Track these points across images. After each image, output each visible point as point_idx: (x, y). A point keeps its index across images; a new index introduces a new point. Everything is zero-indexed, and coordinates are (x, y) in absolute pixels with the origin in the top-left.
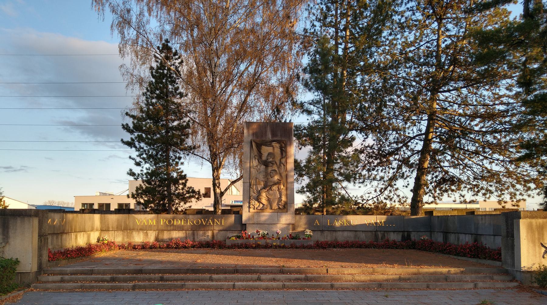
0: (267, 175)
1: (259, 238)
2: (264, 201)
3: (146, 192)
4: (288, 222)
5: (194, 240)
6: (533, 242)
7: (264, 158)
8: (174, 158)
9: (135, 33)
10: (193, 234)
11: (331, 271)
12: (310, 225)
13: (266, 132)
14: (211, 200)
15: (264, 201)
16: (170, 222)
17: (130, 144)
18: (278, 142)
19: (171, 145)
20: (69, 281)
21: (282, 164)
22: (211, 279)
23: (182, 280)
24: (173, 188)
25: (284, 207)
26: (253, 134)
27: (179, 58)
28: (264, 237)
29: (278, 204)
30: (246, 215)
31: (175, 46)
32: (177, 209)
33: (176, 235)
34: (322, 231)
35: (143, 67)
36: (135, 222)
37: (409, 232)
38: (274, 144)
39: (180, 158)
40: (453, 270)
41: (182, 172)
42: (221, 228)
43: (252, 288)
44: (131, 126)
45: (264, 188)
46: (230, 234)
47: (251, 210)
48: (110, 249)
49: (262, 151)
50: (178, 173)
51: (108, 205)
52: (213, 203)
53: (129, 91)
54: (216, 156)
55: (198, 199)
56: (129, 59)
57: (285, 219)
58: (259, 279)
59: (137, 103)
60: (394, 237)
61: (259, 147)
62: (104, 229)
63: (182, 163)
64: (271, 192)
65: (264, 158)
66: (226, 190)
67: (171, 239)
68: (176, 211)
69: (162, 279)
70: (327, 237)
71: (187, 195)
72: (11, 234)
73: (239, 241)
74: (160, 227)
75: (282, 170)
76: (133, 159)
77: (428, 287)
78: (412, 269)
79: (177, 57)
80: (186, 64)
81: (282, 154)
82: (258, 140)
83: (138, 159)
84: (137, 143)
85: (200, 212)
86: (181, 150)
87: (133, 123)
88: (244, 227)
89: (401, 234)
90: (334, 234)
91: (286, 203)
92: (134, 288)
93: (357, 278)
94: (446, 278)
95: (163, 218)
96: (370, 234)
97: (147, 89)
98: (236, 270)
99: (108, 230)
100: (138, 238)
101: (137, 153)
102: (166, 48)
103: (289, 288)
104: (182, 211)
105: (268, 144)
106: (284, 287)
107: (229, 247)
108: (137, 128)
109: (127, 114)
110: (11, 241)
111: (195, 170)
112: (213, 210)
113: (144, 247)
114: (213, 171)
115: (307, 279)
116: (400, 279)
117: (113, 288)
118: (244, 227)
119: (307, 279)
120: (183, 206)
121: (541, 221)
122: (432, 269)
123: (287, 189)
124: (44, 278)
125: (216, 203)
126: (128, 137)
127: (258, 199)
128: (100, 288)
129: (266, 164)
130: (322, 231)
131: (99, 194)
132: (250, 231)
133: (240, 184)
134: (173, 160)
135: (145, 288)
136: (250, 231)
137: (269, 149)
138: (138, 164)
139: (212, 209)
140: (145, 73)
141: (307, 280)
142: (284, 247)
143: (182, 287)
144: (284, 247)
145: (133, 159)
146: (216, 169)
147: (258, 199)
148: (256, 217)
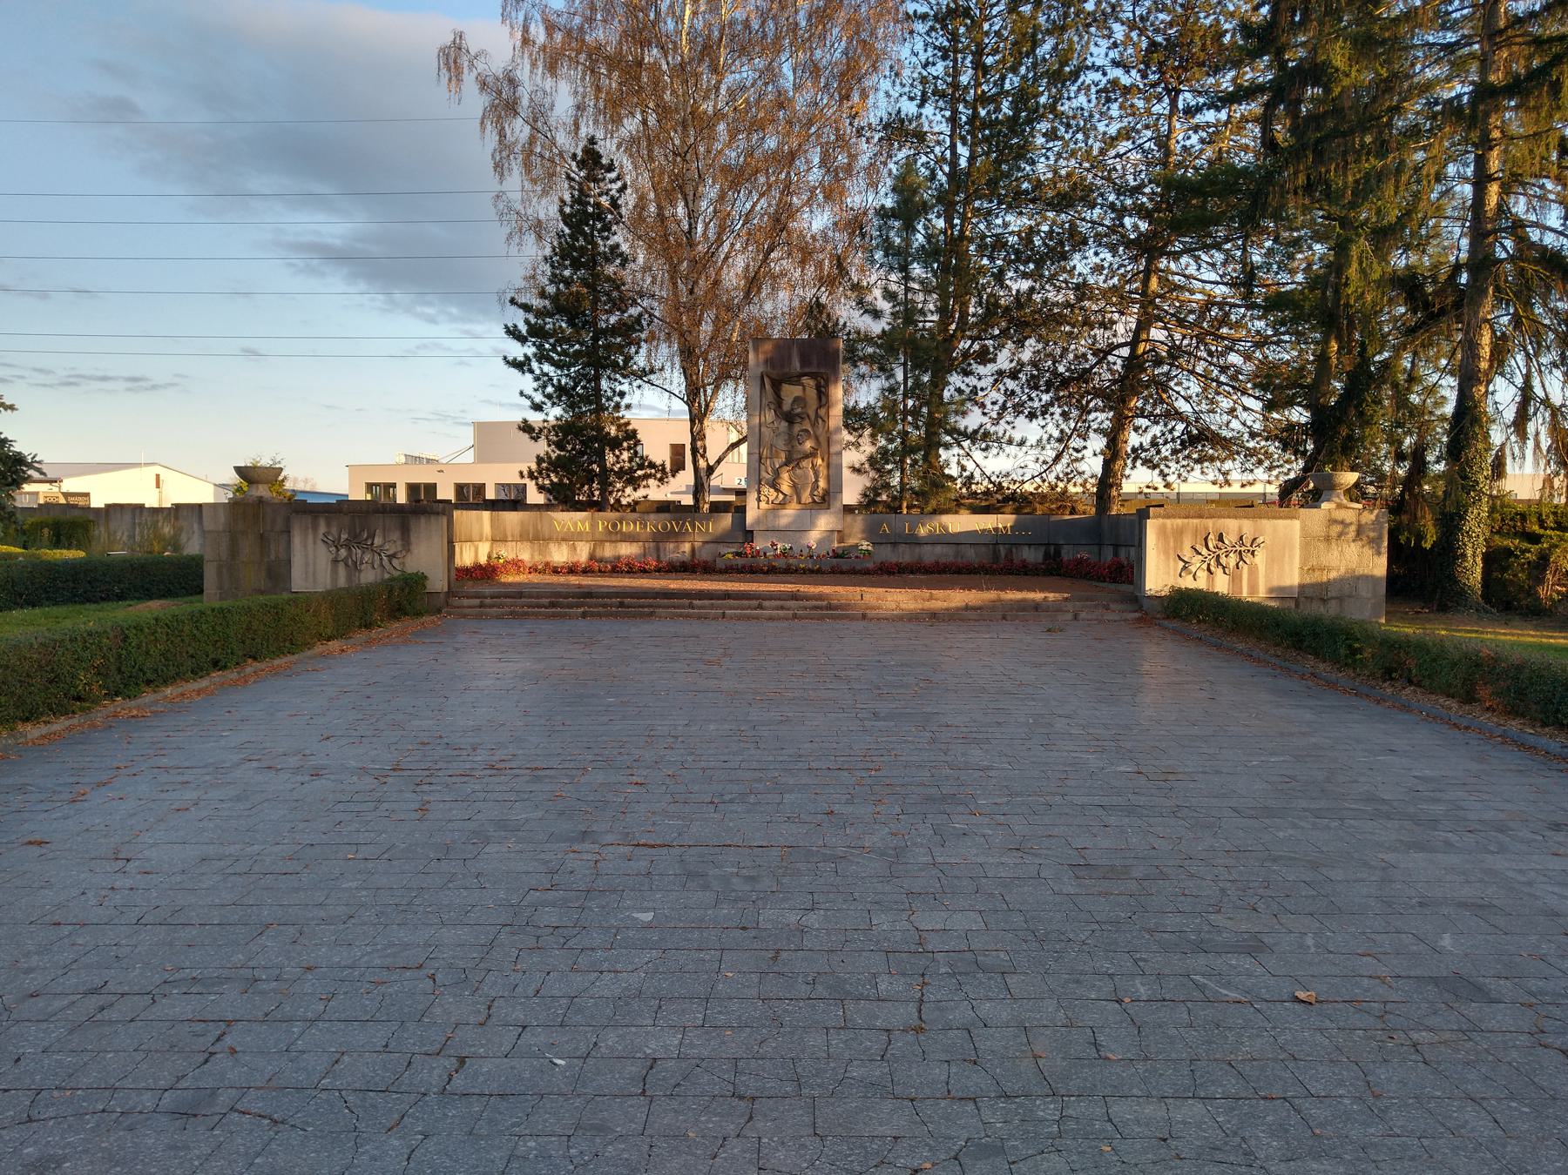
0: (792, 440)
1: (776, 556)
2: (785, 487)
3: (555, 465)
4: (829, 528)
5: (658, 560)
6: (1166, 553)
7: (786, 407)
8: (609, 394)
9: (527, 129)
10: (658, 549)
11: (867, 597)
12: (871, 532)
13: (790, 357)
14: (686, 477)
15: (785, 487)
16: (614, 526)
17: (521, 365)
18: (813, 376)
19: (605, 368)
20: (491, 606)
21: (820, 418)
22: (691, 606)
23: (650, 606)
24: (610, 458)
25: (823, 498)
26: (766, 361)
27: (618, 178)
28: (784, 554)
29: (812, 495)
30: (751, 515)
31: (608, 149)
32: (618, 501)
33: (627, 550)
34: (894, 544)
35: (544, 201)
36: (551, 524)
37: (1058, 548)
38: (805, 380)
39: (622, 394)
40: (1051, 596)
41: (628, 423)
42: (707, 538)
43: (749, 618)
44: (523, 329)
45: (786, 464)
46: (723, 549)
47: (763, 505)
48: (519, 572)
49: (783, 394)
50: (619, 426)
51: (480, 488)
52: (692, 482)
53: (514, 250)
54: (698, 390)
55: (661, 480)
56: (515, 180)
57: (824, 523)
58: (760, 607)
59: (533, 277)
60: (1031, 555)
61: (777, 386)
62: (498, 538)
63: (628, 407)
64: (798, 471)
65: (786, 407)
66: (719, 461)
67: (618, 558)
68: (617, 507)
69: (622, 605)
70: (904, 556)
71: (640, 473)
72: (413, 539)
73: (740, 561)
74: (598, 536)
75: (820, 431)
76: (529, 397)
77: (1004, 618)
78: (991, 595)
79: (613, 175)
80: (631, 183)
81: (820, 398)
82: (774, 373)
83: (538, 398)
84: (535, 365)
85: (664, 507)
86: (624, 377)
87: (527, 322)
88: (749, 535)
89: (1043, 549)
90: (917, 550)
91: (827, 493)
92: (584, 615)
93: (903, 606)
94: (1037, 607)
95: (604, 520)
96: (983, 549)
97: (554, 249)
98: (727, 595)
99: (504, 540)
100: (560, 555)
101: (535, 385)
102: (591, 159)
103: (801, 618)
104: (629, 505)
105: (795, 379)
106: (795, 617)
107: (721, 572)
108: (536, 332)
109: (513, 301)
110: (413, 547)
111: (652, 409)
112: (691, 502)
113: (572, 570)
114: (692, 421)
115: (829, 607)
116: (967, 608)
117: (554, 616)
118: (749, 535)
119: (829, 607)
120: (630, 495)
121: (1179, 521)
122: (1018, 595)
123: (828, 466)
124: (456, 601)
125: (699, 489)
126: (518, 351)
127: (774, 485)
128: (537, 615)
129: (790, 418)
130: (894, 544)
131: (403, 460)
132: (759, 545)
133: (744, 448)
134: (609, 399)
135: (600, 615)
136: (759, 545)
137: (796, 391)
138: (537, 407)
139: (688, 500)
140: (548, 210)
141: (830, 611)
142: (819, 571)
143: (651, 614)
144: (819, 571)
145: (529, 397)
146: (697, 417)
147: (774, 485)
148: (771, 518)
